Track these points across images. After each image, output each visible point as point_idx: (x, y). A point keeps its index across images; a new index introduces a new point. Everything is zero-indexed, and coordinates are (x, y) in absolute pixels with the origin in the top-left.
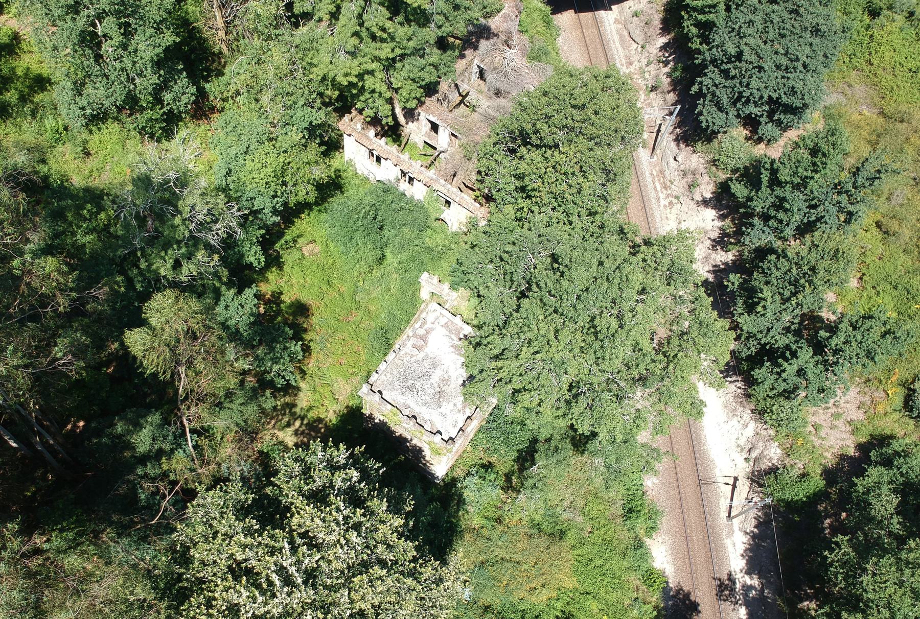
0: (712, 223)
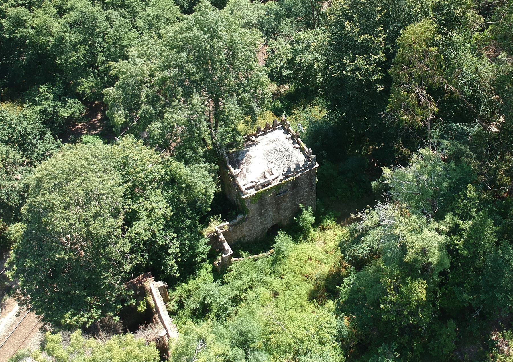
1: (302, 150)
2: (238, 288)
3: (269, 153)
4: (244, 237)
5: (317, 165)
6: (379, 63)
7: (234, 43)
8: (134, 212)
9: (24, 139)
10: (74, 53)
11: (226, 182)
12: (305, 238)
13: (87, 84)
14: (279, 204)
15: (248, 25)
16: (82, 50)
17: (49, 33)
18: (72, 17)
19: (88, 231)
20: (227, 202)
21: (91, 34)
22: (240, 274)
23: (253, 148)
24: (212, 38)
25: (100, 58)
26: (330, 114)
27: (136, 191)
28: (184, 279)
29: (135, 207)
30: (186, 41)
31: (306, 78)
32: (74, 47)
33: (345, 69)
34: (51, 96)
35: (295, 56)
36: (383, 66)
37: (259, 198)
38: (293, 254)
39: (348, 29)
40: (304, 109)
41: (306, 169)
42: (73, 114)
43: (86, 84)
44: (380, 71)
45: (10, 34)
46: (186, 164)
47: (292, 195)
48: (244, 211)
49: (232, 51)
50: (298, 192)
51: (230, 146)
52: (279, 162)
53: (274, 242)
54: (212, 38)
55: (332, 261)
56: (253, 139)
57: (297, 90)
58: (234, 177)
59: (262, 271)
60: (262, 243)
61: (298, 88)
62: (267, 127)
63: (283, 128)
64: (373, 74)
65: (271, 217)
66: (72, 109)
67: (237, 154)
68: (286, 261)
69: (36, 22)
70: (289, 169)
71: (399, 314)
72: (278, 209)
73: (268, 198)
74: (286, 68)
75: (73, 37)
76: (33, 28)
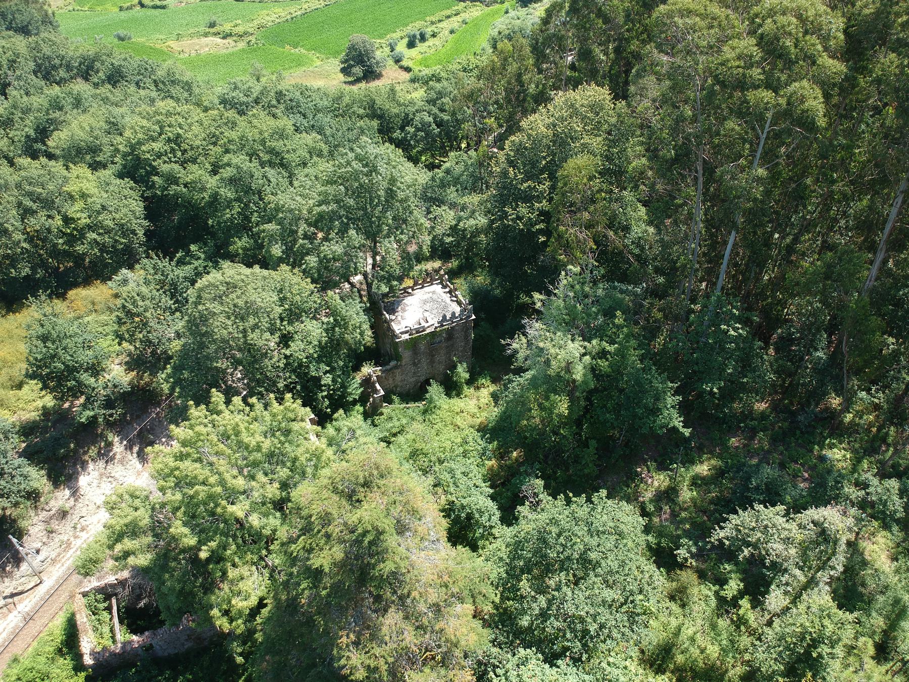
0: (92, 473)
1: (459, 303)
3: (425, 302)
5: (474, 317)
6: (542, 213)
9: (175, 289)
10: (228, 211)
11: (381, 328)
14: (433, 356)
17: (203, 189)
18: (227, 173)
19: (245, 342)
21: (246, 193)
25: (255, 218)
26: (493, 282)
27: (294, 314)
29: (290, 328)
32: (229, 204)
33: (506, 217)
34: (203, 256)
35: (459, 221)
36: (545, 215)
37: (413, 344)
41: (462, 319)
43: (239, 244)
44: (542, 221)
45: (163, 192)
47: (447, 347)
48: (398, 358)
52: (435, 311)
56: (410, 290)
58: (388, 322)
61: (455, 255)
63: (441, 283)
64: (536, 224)
65: (424, 368)
67: (393, 303)
68: (438, 412)
73: (422, 346)
74: (448, 235)
75: (227, 193)
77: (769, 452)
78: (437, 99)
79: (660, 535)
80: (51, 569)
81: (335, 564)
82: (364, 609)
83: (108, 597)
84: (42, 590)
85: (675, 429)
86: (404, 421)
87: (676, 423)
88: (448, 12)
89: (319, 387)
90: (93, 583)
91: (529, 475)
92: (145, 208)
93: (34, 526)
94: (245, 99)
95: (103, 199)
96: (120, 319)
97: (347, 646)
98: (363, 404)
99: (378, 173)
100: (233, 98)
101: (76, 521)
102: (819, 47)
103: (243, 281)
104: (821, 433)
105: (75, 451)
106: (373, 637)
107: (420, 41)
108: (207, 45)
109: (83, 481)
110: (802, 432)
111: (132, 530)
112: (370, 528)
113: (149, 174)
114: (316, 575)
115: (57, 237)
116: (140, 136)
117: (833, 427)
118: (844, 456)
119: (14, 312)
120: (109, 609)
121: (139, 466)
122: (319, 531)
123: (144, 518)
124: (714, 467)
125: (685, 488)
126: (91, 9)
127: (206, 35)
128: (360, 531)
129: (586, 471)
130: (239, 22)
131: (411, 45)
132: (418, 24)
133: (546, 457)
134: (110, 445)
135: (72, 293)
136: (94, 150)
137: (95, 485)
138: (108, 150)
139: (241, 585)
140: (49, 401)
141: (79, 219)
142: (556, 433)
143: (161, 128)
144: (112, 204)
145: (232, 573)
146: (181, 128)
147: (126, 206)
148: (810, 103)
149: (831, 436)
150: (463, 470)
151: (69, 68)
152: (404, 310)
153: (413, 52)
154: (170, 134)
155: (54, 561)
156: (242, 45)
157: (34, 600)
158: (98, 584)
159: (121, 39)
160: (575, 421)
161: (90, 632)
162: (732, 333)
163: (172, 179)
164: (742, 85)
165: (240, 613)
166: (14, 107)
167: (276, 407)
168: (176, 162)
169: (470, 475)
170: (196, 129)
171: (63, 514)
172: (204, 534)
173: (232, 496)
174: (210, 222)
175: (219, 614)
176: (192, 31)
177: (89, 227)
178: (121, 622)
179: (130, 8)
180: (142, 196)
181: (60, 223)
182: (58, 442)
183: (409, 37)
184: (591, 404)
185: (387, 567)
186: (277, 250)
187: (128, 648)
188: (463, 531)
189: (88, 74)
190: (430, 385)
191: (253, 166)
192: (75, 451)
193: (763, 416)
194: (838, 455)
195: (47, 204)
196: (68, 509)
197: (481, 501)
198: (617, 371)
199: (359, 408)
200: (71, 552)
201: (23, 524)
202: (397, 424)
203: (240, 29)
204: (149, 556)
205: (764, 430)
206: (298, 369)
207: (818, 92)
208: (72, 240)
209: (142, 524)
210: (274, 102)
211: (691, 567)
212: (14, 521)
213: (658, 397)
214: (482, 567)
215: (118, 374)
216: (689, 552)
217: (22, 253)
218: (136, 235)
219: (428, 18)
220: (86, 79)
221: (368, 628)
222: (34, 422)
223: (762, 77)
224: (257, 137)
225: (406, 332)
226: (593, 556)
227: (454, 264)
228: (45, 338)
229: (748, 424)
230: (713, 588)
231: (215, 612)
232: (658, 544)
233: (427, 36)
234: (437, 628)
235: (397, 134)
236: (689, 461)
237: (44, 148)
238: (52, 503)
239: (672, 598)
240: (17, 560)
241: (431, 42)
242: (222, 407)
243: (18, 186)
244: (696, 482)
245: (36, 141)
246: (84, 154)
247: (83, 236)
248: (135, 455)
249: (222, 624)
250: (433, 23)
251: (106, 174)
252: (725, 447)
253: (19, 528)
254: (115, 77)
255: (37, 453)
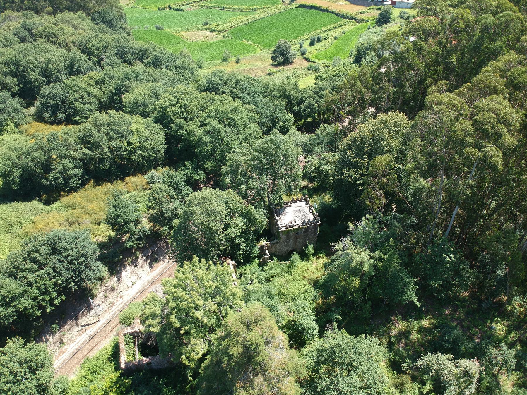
0: (128, 271)
1: (313, 214)
2: (270, 274)
3: (296, 212)
4: (276, 252)
5: (320, 223)
7: (287, 152)
8: (229, 224)
11: (272, 222)
12: (307, 260)
13: (210, 164)
15: (297, 145)
16: (210, 147)
17: (195, 135)
18: (208, 128)
20: (271, 232)
21: (216, 139)
22: (272, 268)
23: (288, 208)
24: (276, 148)
26: (333, 201)
27: (231, 214)
28: (244, 264)
29: (230, 221)
30: (264, 148)
31: (324, 180)
32: (206, 144)
33: (343, 175)
34: (191, 168)
37: (287, 233)
38: (300, 266)
39: (348, 154)
40: (320, 196)
42: (200, 179)
45: (175, 133)
46: (255, 208)
47: (304, 236)
48: (279, 238)
49: (285, 156)
50: (307, 235)
51: (277, 205)
53: (291, 257)
54: (276, 148)
55: (320, 273)
56: (289, 204)
57: (318, 187)
58: (276, 220)
59: (283, 270)
60: (285, 257)
61: (317, 184)
62: (297, 199)
63: (306, 201)
65: (291, 245)
66: (200, 176)
68: (296, 268)
69: (189, 129)
70: (305, 221)
71: (345, 293)
72: (296, 242)
73: (292, 234)
74: (314, 172)
75: (207, 139)
76: (186, 131)
77: (463, 320)
78: (319, 92)
79: (396, 354)
80: (104, 314)
81: (238, 353)
82: (248, 373)
83: (134, 338)
84: (99, 324)
85: (413, 302)
86: (278, 271)
87: (413, 299)
88: (335, 25)
89: (239, 249)
90: (129, 330)
91: (335, 313)
92: (166, 139)
93: (99, 293)
94: (220, 82)
95: (146, 134)
96: (150, 199)
97: (240, 387)
98: (259, 259)
99: (280, 149)
100: (214, 81)
101: (118, 293)
102: (505, 130)
103: (211, 197)
104: (493, 314)
105: (122, 260)
106: (250, 386)
107: (317, 42)
108: (202, 36)
109: (123, 274)
110: (483, 312)
111: (154, 316)
112: (254, 343)
113: (169, 122)
114: (230, 357)
115: (124, 151)
116: (167, 103)
117: (501, 311)
118: (502, 328)
119: (100, 185)
120: (134, 343)
121: (149, 270)
122: (234, 338)
123: (158, 310)
124: (432, 324)
125: (415, 332)
126: (143, 8)
127: (202, 29)
128: (250, 343)
129: (364, 316)
130: (220, 23)
131: (312, 44)
132: (317, 31)
133: (346, 304)
134: (137, 258)
135: (127, 179)
136: (145, 105)
137: (128, 276)
138: (151, 107)
139: (196, 347)
140: (113, 234)
141: (135, 143)
142: (352, 295)
143: (178, 100)
144: (151, 137)
145: (193, 341)
146: (187, 101)
147: (157, 138)
148: (495, 159)
149: (498, 316)
150: (303, 305)
151: (133, 54)
152: (285, 215)
153: (313, 48)
154: (181, 104)
155: (106, 311)
156: (220, 37)
157: (95, 329)
158: (131, 331)
159: (158, 29)
160: (362, 290)
161: (125, 353)
162: (448, 259)
163: (180, 127)
164: (462, 143)
165: (193, 359)
166: (106, 74)
167: (219, 266)
168: (183, 118)
169: (306, 309)
170: (195, 102)
171: (113, 289)
172: (184, 323)
173: (196, 307)
174: (196, 150)
175: (185, 358)
176: (195, 26)
177: (140, 148)
178: (138, 350)
179: (163, 9)
180: (165, 133)
181: (126, 145)
182: (115, 254)
183: (311, 39)
184: (372, 282)
185: (259, 359)
186: (227, 180)
187: (141, 363)
188: (297, 338)
189: (143, 58)
190: (293, 254)
191: (221, 126)
192: (122, 260)
193: (464, 300)
194: (499, 328)
195: (121, 135)
196: (115, 287)
197: (310, 323)
198: (386, 268)
199: (256, 261)
200: (114, 308)
201: (95, 292)
202: (275, 271)
203: (220, 28)
204: (159, 327)
205: (463, 307)
206: (231, 241)
207: (500, 154)
208: (130, 153)
209: (157, 313)
210: (234, 86)
211: (409, 374)
212: (91, 290)
213: (406, 285)
214: (302, 360)
215: (146, 225)
216: (409, 366)
217: (107, 158)
218: (160, 152)
219: (323, 28)
220: (142, 61)
221: (248, 381)
222: (104, 242)
223: (472, 141)
224: (224, 110)
225: (284, 227)
226: (355, 364)
227: (314, 184)
228: (116, 207)
229: (454, 302)
230: (419, 386)
231: (183, 357)
232: (394, 359)
233: (321, 39)
234: (278, 386)
235: (295, 108)
236: (419, 317)
237: (119, 98)
238: (109, 283)
239: (396, 387)
240: (90, 309)
241: (322, 43)
242: (197, 264)
243: (109, 125)
244: (421, 330)
245: (115, 94)
246: (139, 109)
247: (135, 151)
248: (148, 264)
249: (186, 362)
250: (326, 31)
251: (149, 120)
252: (440, 315)
253: (93, 294)
254: (156, 63)
255: (104, 258)
